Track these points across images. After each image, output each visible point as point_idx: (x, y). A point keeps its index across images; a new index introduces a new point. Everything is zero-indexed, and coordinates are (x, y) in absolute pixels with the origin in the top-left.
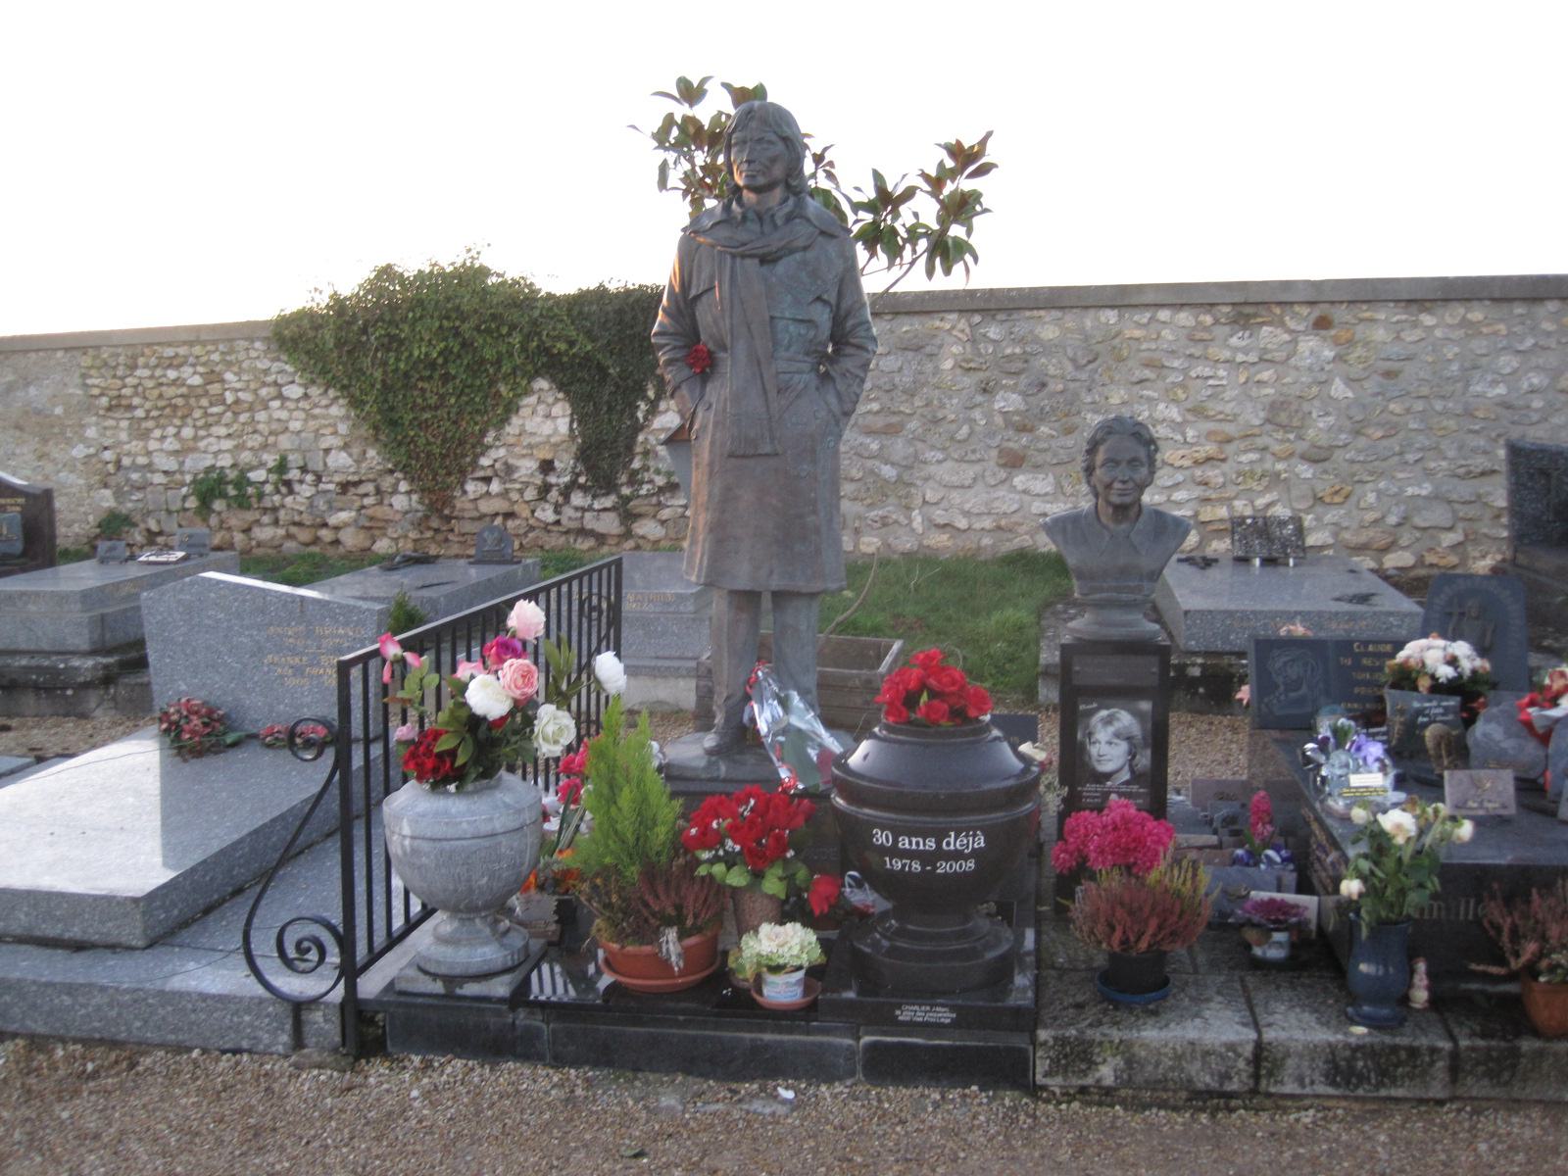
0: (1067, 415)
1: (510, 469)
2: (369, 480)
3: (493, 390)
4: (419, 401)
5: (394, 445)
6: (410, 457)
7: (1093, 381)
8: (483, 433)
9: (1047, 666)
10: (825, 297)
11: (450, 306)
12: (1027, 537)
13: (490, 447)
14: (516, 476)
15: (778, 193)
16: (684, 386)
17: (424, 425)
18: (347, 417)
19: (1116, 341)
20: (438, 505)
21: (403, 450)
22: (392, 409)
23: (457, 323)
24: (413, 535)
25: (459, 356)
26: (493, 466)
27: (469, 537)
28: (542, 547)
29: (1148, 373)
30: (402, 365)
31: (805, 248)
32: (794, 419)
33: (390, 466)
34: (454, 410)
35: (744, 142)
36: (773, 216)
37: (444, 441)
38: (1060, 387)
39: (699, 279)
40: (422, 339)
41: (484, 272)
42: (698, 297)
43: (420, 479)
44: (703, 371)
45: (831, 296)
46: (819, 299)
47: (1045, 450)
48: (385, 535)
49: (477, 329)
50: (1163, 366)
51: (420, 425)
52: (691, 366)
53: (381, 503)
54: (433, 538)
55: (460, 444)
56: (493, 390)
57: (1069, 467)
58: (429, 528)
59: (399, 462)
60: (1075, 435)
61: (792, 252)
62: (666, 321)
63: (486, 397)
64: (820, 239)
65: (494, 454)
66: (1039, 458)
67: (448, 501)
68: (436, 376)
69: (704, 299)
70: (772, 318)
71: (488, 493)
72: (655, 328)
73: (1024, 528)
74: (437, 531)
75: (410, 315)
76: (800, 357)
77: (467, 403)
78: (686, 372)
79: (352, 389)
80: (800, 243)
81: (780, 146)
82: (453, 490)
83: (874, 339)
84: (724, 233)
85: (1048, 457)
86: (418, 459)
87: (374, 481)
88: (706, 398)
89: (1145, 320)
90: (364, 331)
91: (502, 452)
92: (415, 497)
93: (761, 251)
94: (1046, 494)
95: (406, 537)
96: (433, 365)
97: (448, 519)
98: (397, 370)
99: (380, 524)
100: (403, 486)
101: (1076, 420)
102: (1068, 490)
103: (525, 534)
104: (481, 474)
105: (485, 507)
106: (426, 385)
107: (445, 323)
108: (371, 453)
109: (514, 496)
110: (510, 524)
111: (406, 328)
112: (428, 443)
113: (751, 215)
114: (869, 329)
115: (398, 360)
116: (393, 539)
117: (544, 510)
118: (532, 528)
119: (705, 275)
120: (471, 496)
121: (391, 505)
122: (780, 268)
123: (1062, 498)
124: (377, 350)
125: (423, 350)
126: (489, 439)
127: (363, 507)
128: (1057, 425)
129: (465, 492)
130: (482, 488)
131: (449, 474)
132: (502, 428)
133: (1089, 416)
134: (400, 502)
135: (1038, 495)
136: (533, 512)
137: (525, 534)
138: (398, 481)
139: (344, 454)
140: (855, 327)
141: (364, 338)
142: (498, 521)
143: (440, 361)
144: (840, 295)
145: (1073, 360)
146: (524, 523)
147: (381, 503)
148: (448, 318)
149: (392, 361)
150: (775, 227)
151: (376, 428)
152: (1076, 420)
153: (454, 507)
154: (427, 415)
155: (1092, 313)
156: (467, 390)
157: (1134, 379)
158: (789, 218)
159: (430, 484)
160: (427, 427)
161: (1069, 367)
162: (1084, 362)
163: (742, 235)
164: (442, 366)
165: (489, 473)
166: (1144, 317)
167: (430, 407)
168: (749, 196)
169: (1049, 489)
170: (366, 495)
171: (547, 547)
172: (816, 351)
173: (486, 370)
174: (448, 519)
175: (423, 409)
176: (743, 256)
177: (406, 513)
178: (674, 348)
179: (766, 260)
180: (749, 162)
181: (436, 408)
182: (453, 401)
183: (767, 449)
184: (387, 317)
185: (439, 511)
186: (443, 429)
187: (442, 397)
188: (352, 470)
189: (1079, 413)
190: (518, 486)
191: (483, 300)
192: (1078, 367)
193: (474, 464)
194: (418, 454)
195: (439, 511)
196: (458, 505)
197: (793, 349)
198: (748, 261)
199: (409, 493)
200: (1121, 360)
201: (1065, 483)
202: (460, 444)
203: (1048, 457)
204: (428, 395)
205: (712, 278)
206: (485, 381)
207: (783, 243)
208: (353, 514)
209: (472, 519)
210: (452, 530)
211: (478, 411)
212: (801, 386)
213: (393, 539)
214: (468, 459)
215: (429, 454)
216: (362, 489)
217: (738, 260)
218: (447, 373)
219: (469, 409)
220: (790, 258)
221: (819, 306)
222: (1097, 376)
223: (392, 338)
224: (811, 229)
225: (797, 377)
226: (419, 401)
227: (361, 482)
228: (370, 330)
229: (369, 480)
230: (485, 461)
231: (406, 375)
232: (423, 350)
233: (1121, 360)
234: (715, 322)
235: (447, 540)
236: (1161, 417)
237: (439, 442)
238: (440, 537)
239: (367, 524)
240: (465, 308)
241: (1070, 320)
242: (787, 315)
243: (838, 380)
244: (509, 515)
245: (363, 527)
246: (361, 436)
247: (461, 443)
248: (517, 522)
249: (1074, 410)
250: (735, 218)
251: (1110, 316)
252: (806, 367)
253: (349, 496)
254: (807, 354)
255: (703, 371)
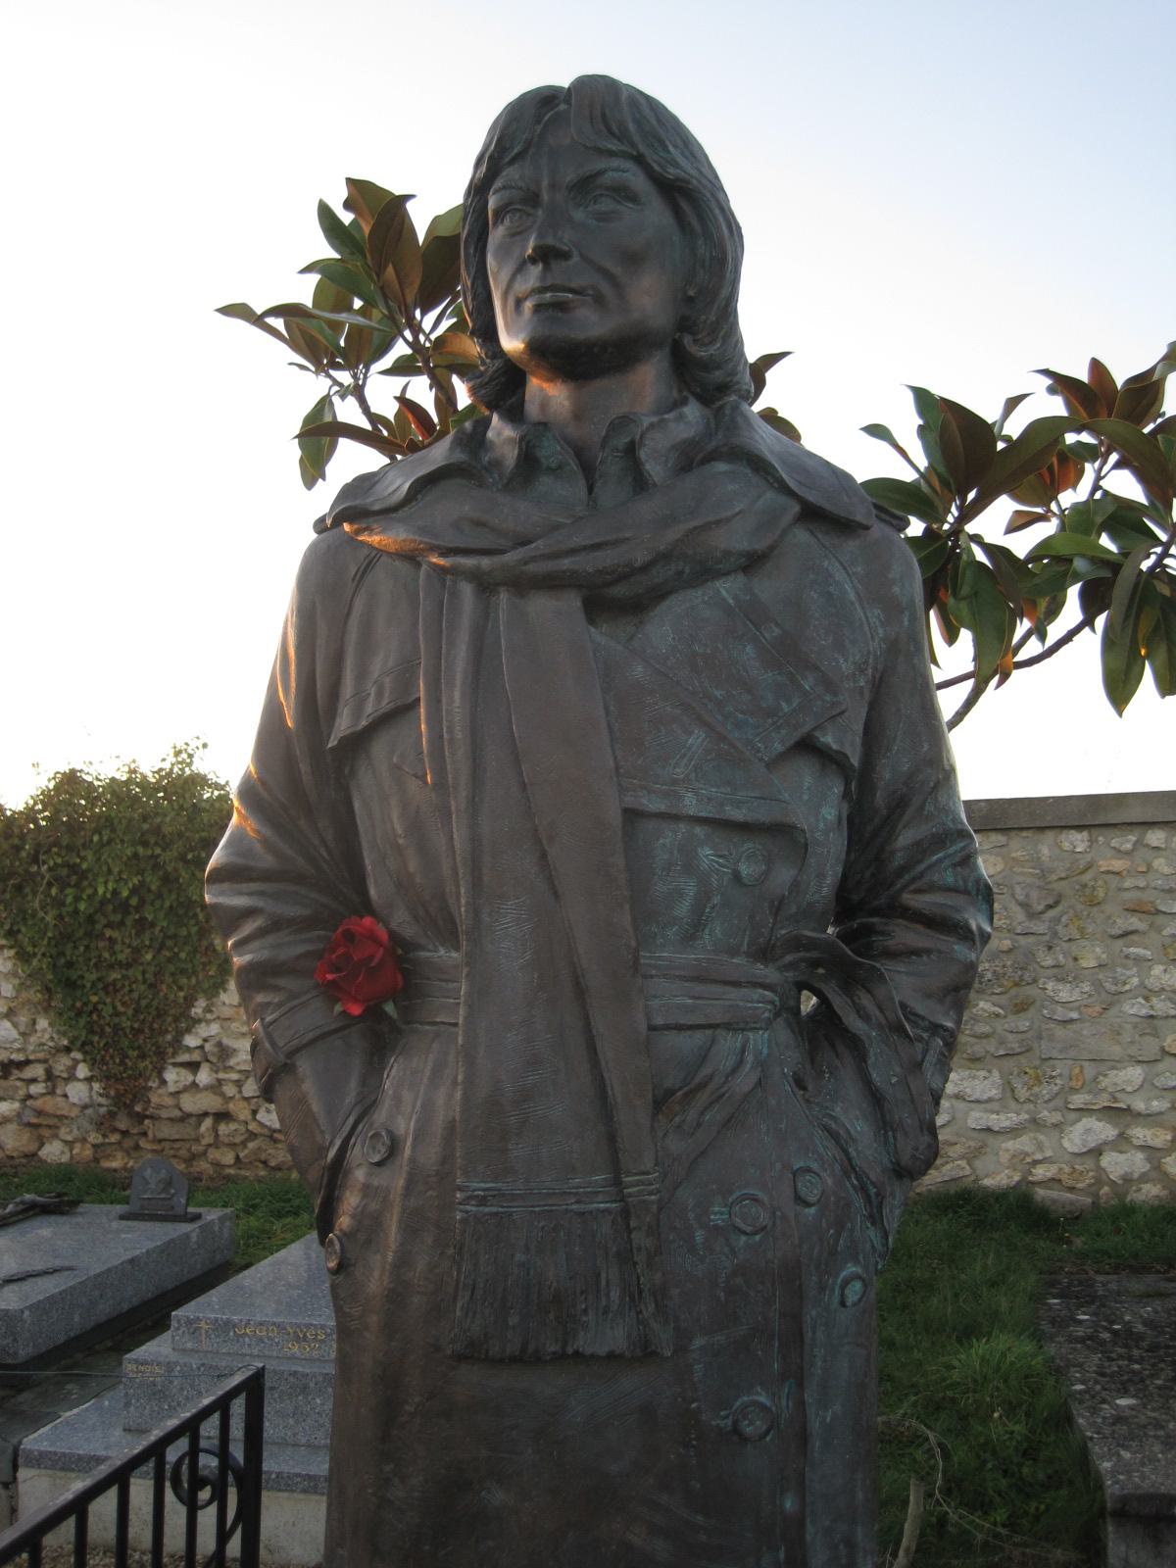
0: (1017, 985)
1: (225, 1052)
2: (39, 1061)
3: (205, 943)
4: (106, 955)
5: (72, 1014)
6: (92, 1032)
7: (1056, 934)
8: (190, 1001)
9: (1124, 1500)
10: (828, 739)
11: (146, 826)
12: (963, 1163)
13: (199, 1021)
14: (232, 1062)
15: (650, 378)
16: (304, 1065)
17: (110, 989)
18: (15, 975)
19: (1087, 877)
20: (127, 1098)
21: (82, 1022)
22: (70, 965)
23: (158, 851)
24: (94, 1138)
25: (160, 896)
26: (201, 1047)
27: (167, 1145)
28: (265, 1163)
29: (1135, 922)
30: (82, 906)
31: (752, 563)
32: (718, 1215)
33: (66, 1042)
34: (152, 969)
35: (532, 199)
36: (631, 450)
37: (137, 1011)
38: (1007, 944)
39: (361, 675)
40: (110, 872)
41: (199, 780)
42: (357, 742)
43: (103, 1061)
44: (374, 1013)
45: (844, 739)
46: (807, 746)
47: (987, 1036)
48: (56, 1136)
49: (182, 858)
50: (1158, 912)
51: (105, 988)
52: (332, 992)
53: (52, 1092)
54: (119, 1143)
55: (159, 1016)
56: (205, 943)
57: (1022, 1059)
58: (115, 1130)
59: (76, 1038)
60: (1031, 1012)
61: (705, 572)
62: (252, 827)
63: (195, 951)
64: (801, 535)
65: (203, 1031)
66: (979, 1049)
67: (141, 1094)
68: (129, 921)
69: (380, 749)
70: (632, 815)
71: (194, 1084)
72: (217, 858)
73: (958, 1150)
74: (125, 1133)
75: (96, 838)
76: (740, 965)
77: (169, 960)
78: (315, 1016)
79: (20, 937)
80: (737, 539)
81: (655, 215)
82: (147, 1079)
83: (985, 895)
84: (452, 507)
85: (991, 1046)
86: (102, 1034)
87: (45, 1061)
88: (380, 1116)
89: (1129, 846)
90: (35, 859)
91: (214, 1029)
92: (96, 1086)
93: (588, 563)
94: (990, 1100)
95: (84, 1140)
96: (124, 907)
97: (140, 1118)
98: (76, 912)
99: (51, 1121)
100: (82, 1071)
101: (1032, 991)
102: (1023, 1093)
103: (244, 1144)
104: (185, 1057)
105: (190, 1103)
106: (116, 934)
107: (141, 850)
108: (43, 1023)
109: (230, 1090)
110: (224, 1129)
111: (90, 855)
112: (116, 1014)
113: (550, 451)
114: (967, 860)
115: (77, 899)
116: (66, 1142)
117: (268, 1111)
118: (253, 1136)
119: (382, 663)
120: (172, 1088)
121: (66, 1096)
122: (662, 629)
123: (1013, 1105)
124: (50, 885)
125: (110, 886)
126: (197, 1010)
127: (30, 1097)
128: (1003, 1000)
129: (164, 1082)
130: (186, 1077)
131: (143, 1056)
132: (217, 995)
133: (1050, 986)
134: (77, 1092)
135: (978, 1101)
136: (255, 1112)
137: (244, 1144)
138: (76, 1062)
139: (7, 1024)
140: (921, 849)
141: (34, 868)
142: (208, 1122)
143: (134, 901)
144: (872, 735)
145: (1025, 905)
146: (242, 1128)
147: (52, 1092)
148: (145, 844)
149: (69, 900)
150: (640, 483)
151: (47, 989)
152: (1032, 991)
153: (149, 1101)
154: (115, 975)
155: (1050, 835)
156: (169, 943)
157: (1116, 931)
158: (691, 458)
159: (116, 1070)
160: (116, 991)
161: (1019, 915)
162: (1041, 908)
163: (517, 512)
164: (138, 909)
165: (196, 1057)
166: (1127, 841)
167: (120, 964)
168: (547, 394)
169: (994, 1093)
170: (34, 1080)
171: (273, 1164)
172: (796, 943)
173: (195, 915)
174: (140, 1118)
175: (111, 966)
176: (522, 584)
177: (85, 1107)
178: (276, 925)
179: (614, 599)
180: (545, 255)
181: (128, 966)
182: (149, 957)
183: (615, 1337)
184: (65, 841)
185: (129, 1107)
186: (135, 995)
187: (136, 951)
188: (17, 1045)
189: (1035, 981)
190: (235, 1076)
191: (191, 819)
192: (1032, 915)
193: (177, 1045)
194: (103, 1030)
195: (129, 1107)
196: (154, 1099)
197: (716, 931)
198: (542, 607)
199: (89, 1080)
200: (1094, 903)
201: (1017, 1084)
202: (159, 1016)
203: (991, 1046)
204: (118, 947)
205: (405, 674)
206: (194, 930)
207: (674, 534)
208: (16, 1105)
209: (171, 1120)
210: (145, 1134)
211: (183, 972)
212: (745, 1081)
213: (66, 1142)
214: (169, 1037)
215: (116, 1028)
216: (28, 1073)
217: (504, 597)
218: (143, 919)
219: (172, 968)
220: (697, 597)
221: (806, 773)
222: (1059, 928)
223: (73, 868)
224: (770, 496)
225: (729, 1042)
226: (106, 955)
227: (28, 1062)
228: (42, 857)
229: (39, 1061)
230: (191, 1041)
231: (91, 919)
232: (110, 886)
233: (1094, 903)
234: (415, 826)
235: (137, 1147)
236: (1156, 986)
237: (130, 1012)
238: (128, 1143)
239: (34, 1120)
240: (167, 830)
241: (1018, 847)
242: (690, 804)
243: (875, 1052)
244: (223, 1116)
245: (29, 1125)
246: (29, 1001)
247: (160, 1014)
248: (233, 1126)
249: (1027, 977)
250: (497, 464)
251: (1078, 841)
252: (759, 1002)
253: (12, 1081)
254: (764, 953)
255: (374, 1013)
